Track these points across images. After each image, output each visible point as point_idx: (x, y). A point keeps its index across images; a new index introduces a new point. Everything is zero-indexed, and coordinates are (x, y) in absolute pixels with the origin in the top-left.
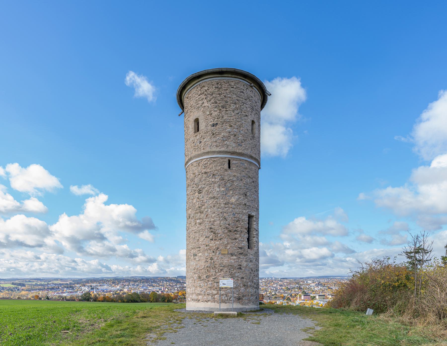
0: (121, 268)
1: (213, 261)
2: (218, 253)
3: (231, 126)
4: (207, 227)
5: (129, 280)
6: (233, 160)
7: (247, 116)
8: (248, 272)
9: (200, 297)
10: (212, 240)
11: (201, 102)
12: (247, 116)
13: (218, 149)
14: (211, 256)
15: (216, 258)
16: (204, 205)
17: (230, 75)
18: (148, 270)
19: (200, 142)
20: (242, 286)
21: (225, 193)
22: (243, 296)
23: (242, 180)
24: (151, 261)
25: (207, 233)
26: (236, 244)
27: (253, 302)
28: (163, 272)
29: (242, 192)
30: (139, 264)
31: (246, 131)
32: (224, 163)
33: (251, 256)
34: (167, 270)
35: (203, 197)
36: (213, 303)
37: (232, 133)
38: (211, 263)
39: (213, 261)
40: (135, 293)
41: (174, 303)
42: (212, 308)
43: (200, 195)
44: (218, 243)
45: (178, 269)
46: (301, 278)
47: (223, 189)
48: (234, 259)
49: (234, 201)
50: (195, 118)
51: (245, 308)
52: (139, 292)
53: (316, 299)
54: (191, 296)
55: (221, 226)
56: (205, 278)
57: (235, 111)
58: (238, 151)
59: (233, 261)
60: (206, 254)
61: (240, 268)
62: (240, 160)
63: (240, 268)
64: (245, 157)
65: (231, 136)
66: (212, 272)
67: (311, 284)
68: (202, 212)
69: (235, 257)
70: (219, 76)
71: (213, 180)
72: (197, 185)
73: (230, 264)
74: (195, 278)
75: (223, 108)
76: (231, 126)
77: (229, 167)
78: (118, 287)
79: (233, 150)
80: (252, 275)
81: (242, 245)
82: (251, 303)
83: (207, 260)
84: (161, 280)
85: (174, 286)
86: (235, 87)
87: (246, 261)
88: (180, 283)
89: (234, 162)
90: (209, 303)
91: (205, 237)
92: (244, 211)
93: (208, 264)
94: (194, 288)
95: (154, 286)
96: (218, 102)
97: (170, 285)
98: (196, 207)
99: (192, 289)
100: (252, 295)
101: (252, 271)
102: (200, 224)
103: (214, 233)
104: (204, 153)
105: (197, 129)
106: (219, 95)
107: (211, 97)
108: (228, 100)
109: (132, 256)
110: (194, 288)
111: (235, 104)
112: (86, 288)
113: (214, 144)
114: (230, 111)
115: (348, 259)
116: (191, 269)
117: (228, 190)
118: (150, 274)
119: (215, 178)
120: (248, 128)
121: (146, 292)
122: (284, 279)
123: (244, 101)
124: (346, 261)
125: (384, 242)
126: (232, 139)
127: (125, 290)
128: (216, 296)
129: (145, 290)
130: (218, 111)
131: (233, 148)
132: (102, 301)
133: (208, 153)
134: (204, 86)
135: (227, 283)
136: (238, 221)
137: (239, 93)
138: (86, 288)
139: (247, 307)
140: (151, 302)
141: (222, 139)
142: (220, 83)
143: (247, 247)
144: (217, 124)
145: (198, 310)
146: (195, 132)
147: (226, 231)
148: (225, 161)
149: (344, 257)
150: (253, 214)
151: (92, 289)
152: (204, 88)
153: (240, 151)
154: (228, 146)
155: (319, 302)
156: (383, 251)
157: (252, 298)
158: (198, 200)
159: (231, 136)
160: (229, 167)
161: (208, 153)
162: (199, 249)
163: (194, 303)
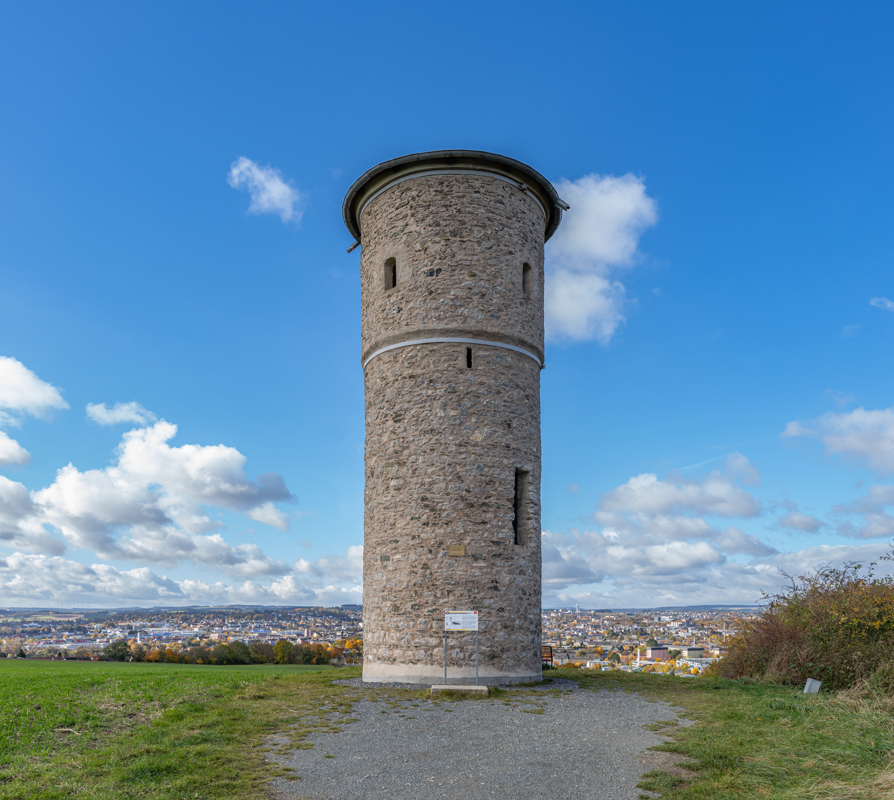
0: (204, 586)
1: (428, 572)
2: (440, 555)
3: (474, 275)
4: (415, 496)
5: (224, 614)
6: (479, 349)
7: (511, 253)
8: (514, 597)
9: (397, 652)
10: (426, 524)
11: (400, 224)
12: (511, 253)
13: (442, 326)
14: (425, 561)
15: (436, 566)
16: (408, 447)
17: (471, 166)
18: (269, 590)
20: (499, 627)
21: (457, 422)
22: (502, 651)
23: (499, 393)
24: (277, 571)
25: (414, 509)
26: (486, 535)
27: (527, 664)
28: (306, 595)
29: (498, 418)
30: (249, 577)
31: (511, 286)
32: (456, 354)
33: (522, 562)
34: (317, 591)
35: (405, 430)
36: (429, 666)
37: (476, 290)
38: (424, 576)
39: (428, 572)
40: (236, 643)
41: (334, 665)
42: (426, 678)
43: (398, 425)
44: (442, 531)
45: (344, 590)
46: (644, 611)
47: (453, 413)
48: (481, 568)
49: (479, 440)
50: (386, 257)
51: (508, 677)
52: (247, 640)
53: (682, 657)
54: (375, 651)
55: (448, 494)
56: (409, 609)
57: (484, 243)
58: (489, 329)
59: (478, 573)
60: (413, 556)
61: (496, 588)
62: (496, 348)
63: (496, 588)
64: (508, 343)
65: (474, 297)
67: (669, 623)
68: (401, 464)
69: (483, 564)
70: (446, 166)
71: (430, 392)
72: (391, 403)
73: (470, 579)
74: (386, 609)
75: (455, 235)
76: (474, 275)
77: (469, 365)
78: (196, 630)
79: (479, 327)
80: (525, 603)
81: (500, 535)
82: (523, 666)
83: (415, 570)
84: (303, 613)
85: (334, 627)
87: (510, 572)
88: (349, 620)
89: (481, 353)
90: (419, 666)
91: (409, 518)
92: (505, 461)
93: (418, 579)
94: (382, 632)
95: (284, 628)
96: (441, 222)
97: (323, 625)
98: (388, 452)
99: (377, 635)
100: (524, 649)
101: (525, 594)
102: (399, 489)
103: (432, 510)
104: (408, 333)
105: (392, 281)
106: (444, 209)
107: (427, 212)
108: (466, 220)
109: (231, 560)
110: (382, 632)
111: (484, 226)
112: (118, 632)
113: (433, 313)
115: (758, 568)
116: (375, 590)
117: (466, 414)
118: (275, 601)
120: (514, 280)
121: (264, 640)
122: (602, 611)
123: (504, 221)
124: (754, 573)
125: (846, 531)
126: (475, 304)
127: (214, 636)
129: (261, 635)
130: (443, 243)
131: (478, 322)
132: (156, 661)
133: (418, 333)
134: (408, 189)
135: (464, 620)
136: (490, 482)
137: (492, 203)
138: (118, 632)
139: (512, 675)
140: (277, 663)
141: (451, 303)
142: (446, 183)
143: (512, 540)
144: (439, 271)
145: (391, 681)
146: (387, 288)
147: (462, 506)
148: (459, 352)
149: (750, 563)
150: (527, 467)
151: (131, 633)
153: (496, 330)
154: (466, 318)
155: (690, 663)
156: (844, 549)
157: (524, 654)
158: (394, 437)
159: (474, 297)
160: (469, 365)
161: (418, 333)
162: (394, 545)
163: (383, 666)
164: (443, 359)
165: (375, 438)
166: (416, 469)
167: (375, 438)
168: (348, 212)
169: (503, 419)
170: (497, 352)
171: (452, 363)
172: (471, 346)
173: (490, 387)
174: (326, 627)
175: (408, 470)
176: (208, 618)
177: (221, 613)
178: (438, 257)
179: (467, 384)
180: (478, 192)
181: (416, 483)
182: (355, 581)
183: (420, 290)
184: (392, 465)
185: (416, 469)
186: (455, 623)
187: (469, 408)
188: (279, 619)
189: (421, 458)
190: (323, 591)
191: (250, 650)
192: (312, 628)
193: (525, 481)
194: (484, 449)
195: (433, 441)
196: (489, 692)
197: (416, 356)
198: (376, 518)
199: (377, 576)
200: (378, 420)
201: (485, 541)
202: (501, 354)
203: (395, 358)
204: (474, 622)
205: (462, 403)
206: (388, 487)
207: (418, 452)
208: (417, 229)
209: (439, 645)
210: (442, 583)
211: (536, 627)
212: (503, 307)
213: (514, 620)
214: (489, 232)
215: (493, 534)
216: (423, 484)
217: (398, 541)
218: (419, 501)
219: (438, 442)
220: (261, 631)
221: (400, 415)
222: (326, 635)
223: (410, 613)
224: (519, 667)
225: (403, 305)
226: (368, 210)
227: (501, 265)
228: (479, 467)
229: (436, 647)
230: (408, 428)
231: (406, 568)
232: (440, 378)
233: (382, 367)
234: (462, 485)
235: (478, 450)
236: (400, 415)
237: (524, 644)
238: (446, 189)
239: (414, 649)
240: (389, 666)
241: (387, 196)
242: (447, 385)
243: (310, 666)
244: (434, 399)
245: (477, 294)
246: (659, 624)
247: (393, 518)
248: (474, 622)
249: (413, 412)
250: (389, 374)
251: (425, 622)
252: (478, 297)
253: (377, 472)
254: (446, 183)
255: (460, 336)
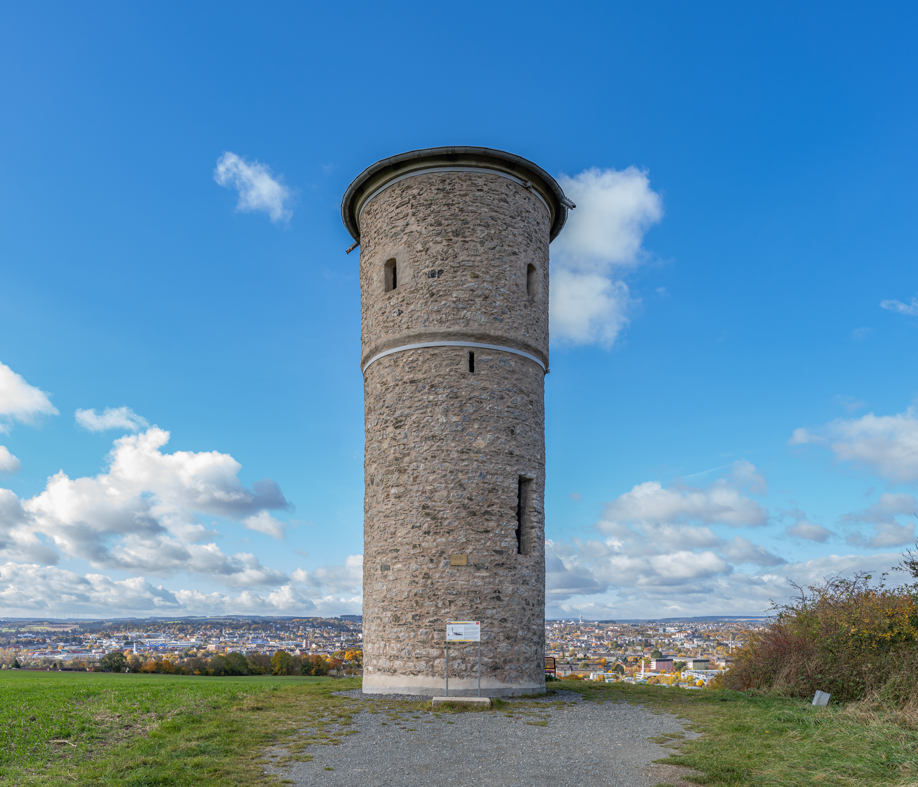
0: (200, 597)
1: (429, 582)
2: (442, 564)
3: (477, 277)
4: (416, 504)
5: (221, 624)
6: (482, 353)
7: (515, 253)
8: (517, 608)
9: (398, 664)
10: (427, 533)
11: (401, 223)
12: (515, 253)
13: (443, 329)
14: (426, 570)
15: (437, 575)
16: (409, 454)
17: (474, 163)
18: (267, 600)
19: (400, 312)
20: (502, 638)
21: (459, 428)
22: (505, 662)
23: (502, 398)
24: (274, 581)
25: (415, 517)
26: (488, 544)
27: (530, 676)
28: (304, 605)
29: (502, 424)
30: (246, 587)
31: (514, 288)
32: (458, 359)
33: (525, 572)
34: (316, 602)
35: (406, 437)
36: (430, 678)
37: (478, 292)
38: (425, 586)
39: (429, 582)
40: (234, 654)
41: (333, 676)
42: (427, 689)
43: (398, 431)
44: (444, 540)
45: (342, 600)
46: (649, 622)
47: (455, 419)
48: (483, 578)
51: (510, 689)
52: (244, 651)
53: (687, 669)
54: (375, 662)
55: (450, 502)
56: (410, 620)
57: (487, 243)
58: (492, 333)
59: (480, 583)
60: (414, 566)
61: (498, 598)
62: (499, 352)
63: (498, 598)
64: (512, 347)
66: (429, 607)
67: (674, 634)
68: (402, 471)
69: (485, 574)
71: (431, 397)
72: (392, 409)
75: (457, 235)
76: (477, 277)
77: (472, 369)
78: (193, 640)
79: (482, 330)
80: (528, 613)
81: (503, 544)
82: (526, 678)
83: (416, 579)
84: (301, 624)
86: (485, 188)
87: (513, 582)
88: (349, 630)
89: (484, 357)
90: (420, 677)
91: (409, 526)
92: (508, 469)
93: (419, 589)
94: (382, 643)
95: (282, 639)
96: (443, 221)
97: (322, 636)
98: (388, 459)
99: (377, 645)
100: (527, 660)
102: (399, 497)
103: (433, 519)
104: (409, 337)
105: (392, 282)
106: (445, 208)
107: (428, 211)
108: (469, 219)
109: (228, 570)
110: (382, 643)
111: (487, 226)
112: (113, 643)
114: (473, 244)
115: (766, 578)
116: (375, 600)
117: (468, 420)
119: (436, 394)
120: (518, 281)
121: (262, 651)
122: (606, 622)
124: (761, 583)
125: (855, 540)
126: (478, 306)
127: (211, 647)
128: (437, 661)
129: (259, 646)
130: (445, 243)
131: (481, 325)
132: (153, 672)
133: (419, 337)
134: (409, 187)
135: (467, 631)
137: (496, 202)
138: (113, 643)
139: (515, 686)
140: (276, 674)
141: (453, 305)
142: (448, 181)
143: (516, 550)
144: (441, 272)
147: (464, 514)
148: (461, 356)
149: (757, 574)
150: (531, 475)
151: (127, 644)
152: (410, 192)
153: (500, 333)
154: (468, 321)
155: (695, 675)
156: (853, 560)
158: (394, 443)
160: (472, 369)
161: (419, 337)
162: (395, 554)
163: (383, 677)
164: (445, 363)
165: (375, 445)
166: (417, 477)
167: (375, 445)
168: (347, 211)
169: (506, 425)
170: (501, 356)
171: (454, 367)
172: (473, 350)
173: (493, 392)
174: (325, 637)
175: (409, 477)
176: (205, 629)
177: (218, 623)
178: (439, 257)
179: (469, 389)
180: (481, 190)
181: (417, 491)
182: (354, 591)
183: (421, 292)
184: (392, 472)
185: (417, 477)
186: (456, 634)
187: (471, 414)
188: (277, 629)
189: (422, 465)
190: (322, 601)
191: (248, 661)
192: (311, 639)
193: (529, 489)
194: (486, 455)
195: (434, 448)
196: (492, 704)
197: (417, 360)
198: (376, 527)
199: (378, 586)
200: (378, 426)
201: (487, 551)
202: (505, 359)
203: (395, 362)
204: (476, 633)
205: (465, 409)
206: (388, 495)
207: (420, 459)
208: (419, 229)
209: (441, 656)
210: (444, 593)
211: (540, 638)
212: (507, 310)
213: (517, 631)
214: (493, 232)
215: (496, 543)
216: (424, 492)
217: (398, 550)
218: (420, 509)
219: (439, 448)
220: (259, 641)
221: (401, 421)
222: (324, 646)
223: (411, 623)
224: (522, 678)
225: (404, 307)
226: (368, 209)
227: (504, 266)
228: (481, 474)
229: (437, 658)
230: (409, 434)
231: (406, 577)
232: (442, 383)
233: (382, 372)
234: (465, 493)
235: (480, 457)
236: (401, 421)
237: (527, 655)
238: (448, 187)
239: (415, 660)
240: (389, 678)
241: (388, 194)
242: (449, 390)
243: (308, 677)
244: (436, 405)
245: (479, 296)
246: (664, 636)
247: (393, 526)
248: (476, 633)
249: (414, 418)
250: (389, 379)
251: (427, 633)
252: (481, 299)
253: (377, 480)
254: (448, 181)
255: (462, 339)
